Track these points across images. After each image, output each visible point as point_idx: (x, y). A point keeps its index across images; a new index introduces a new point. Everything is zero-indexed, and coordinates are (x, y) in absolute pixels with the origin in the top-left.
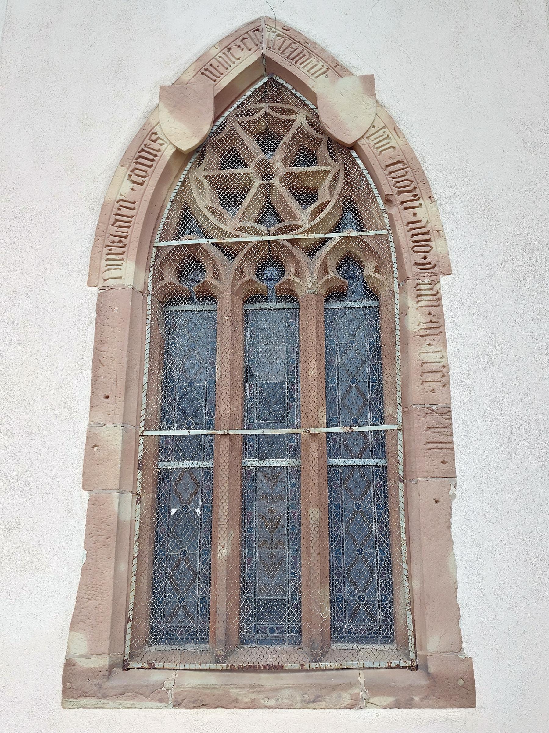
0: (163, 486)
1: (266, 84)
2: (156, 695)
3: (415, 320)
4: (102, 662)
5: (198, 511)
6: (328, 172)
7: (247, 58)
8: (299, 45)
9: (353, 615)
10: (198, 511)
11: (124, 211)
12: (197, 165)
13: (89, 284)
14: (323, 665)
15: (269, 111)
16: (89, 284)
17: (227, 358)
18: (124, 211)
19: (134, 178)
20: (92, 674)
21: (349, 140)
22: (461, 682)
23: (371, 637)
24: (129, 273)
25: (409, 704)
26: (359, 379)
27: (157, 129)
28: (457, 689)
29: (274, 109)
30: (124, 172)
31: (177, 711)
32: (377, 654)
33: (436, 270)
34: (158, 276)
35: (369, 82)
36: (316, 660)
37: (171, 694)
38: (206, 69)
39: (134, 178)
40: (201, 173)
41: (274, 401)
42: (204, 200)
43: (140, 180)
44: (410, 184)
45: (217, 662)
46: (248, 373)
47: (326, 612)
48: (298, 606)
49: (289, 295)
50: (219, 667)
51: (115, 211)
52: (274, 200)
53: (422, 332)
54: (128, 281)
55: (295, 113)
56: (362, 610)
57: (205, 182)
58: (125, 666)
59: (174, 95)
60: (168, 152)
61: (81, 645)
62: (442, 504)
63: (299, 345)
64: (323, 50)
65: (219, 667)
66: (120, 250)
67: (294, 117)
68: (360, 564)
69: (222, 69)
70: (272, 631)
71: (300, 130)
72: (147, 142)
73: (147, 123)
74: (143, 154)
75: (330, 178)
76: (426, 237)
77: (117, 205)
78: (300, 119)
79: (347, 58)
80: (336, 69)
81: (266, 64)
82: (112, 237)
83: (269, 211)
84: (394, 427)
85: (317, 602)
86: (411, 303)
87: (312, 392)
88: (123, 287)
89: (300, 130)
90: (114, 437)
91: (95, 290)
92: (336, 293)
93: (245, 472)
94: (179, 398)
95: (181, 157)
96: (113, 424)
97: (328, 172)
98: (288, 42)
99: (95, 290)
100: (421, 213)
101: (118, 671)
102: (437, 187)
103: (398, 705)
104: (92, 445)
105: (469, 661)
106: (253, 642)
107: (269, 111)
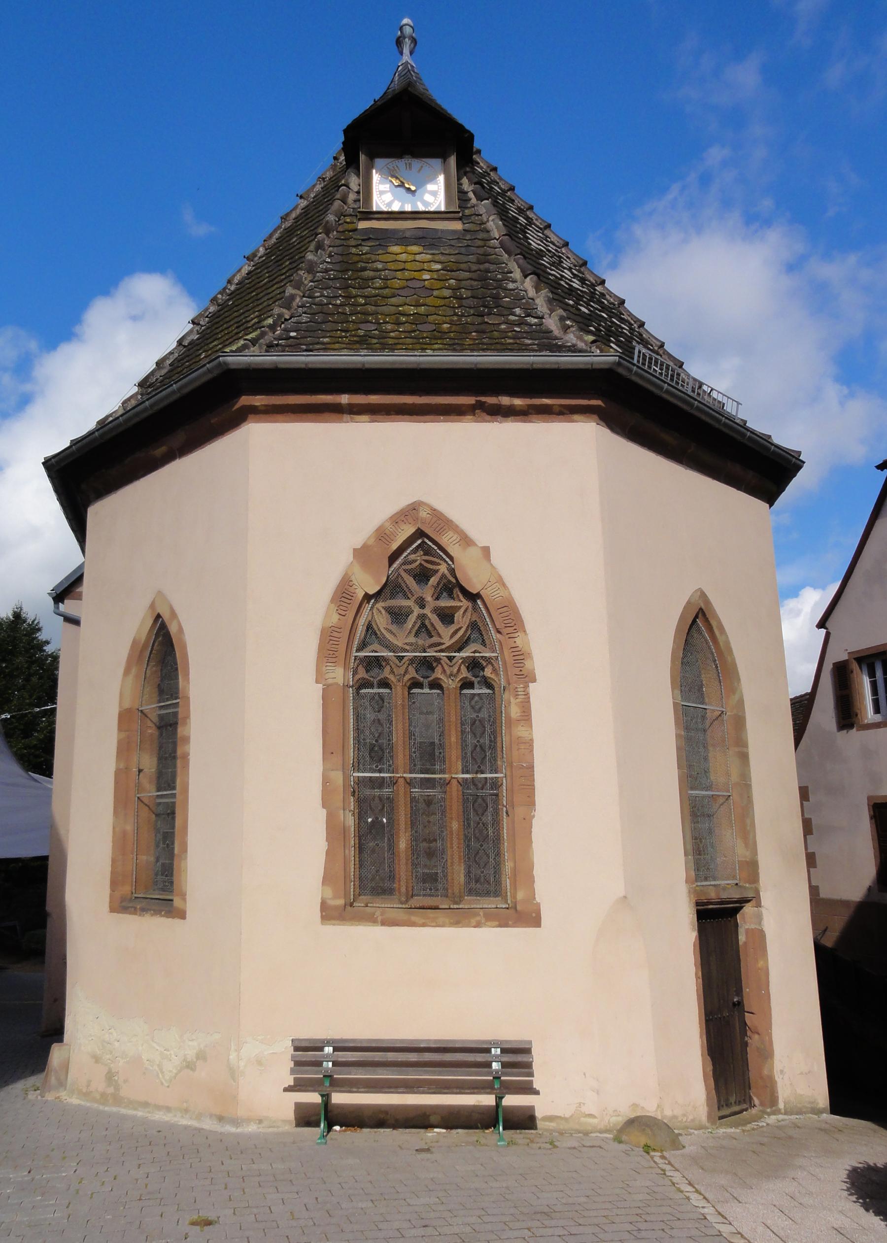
0: (363, 806)
1: (420, 544)
2: (371, 920)
3: (515, 711)
4: (341, 902)
5: (385, 820)
6: (460, 607)
7: (408, 530)
8: (442, 521)
9: (477, 881)
10: (385, 820)
11: (335, 634)
12: (376, 602)
13: (317, 682)
14: (461, 906)
15: (423, 562)
16: (317, 682)
17: (400, 726)
18: (335, 634)
19: (340, 611)
20: (336, 908)
21: (475, 592)
22: (534, 915)
23: (487, 894)
24: (339, 675)
25: (506, 925)
26: (482, 741)
27: (353, 578)
28: (531, 918)
29: (427, 561)
30: (334, 607)
31: (383, 927)
32: (490, 903)
33: (526, 679)
34: (355, 673)
35: (486, 551)
36: (456, 903)
37: (379, 919)
38: (382, 535)
39: (340, 611)
40: (380, 605)
41: (429, 755)
42: (382, 621)
43: (344, 613)
44: (513, 621)
45: (402, 903)
46: (411, 734)
47: (462, 879)
48: (445, 876)
49: (436, 685)
50: (404, 906)
51: (329, 634)
52: (427, 622)
53: (519, 718)
54: (340, 681)
55: (439, 564)
56: (482, 880)
57: (383, 612)
58: (351, 905)
59: (362, 554)
60: (360, 595)
61: (329, 893)
62: (528, 821)
63: (475, 871)
64: (457, 526)
65: (404, 906)
66: (334, 660)
67: (439, 567)
68: (481, 852)
69: (392, 537)
70: (431, 889)
71: (443, 575)
72: (346, 587)
73: (346, 574)
74: (344, 595)
75: (462, 610)
76: (521, 657)
77: (330, 630)
78: (443, 568)
79: (473, 533)
80: (466, 541)
81: (420, 533)
82: (328, 647)
83: (424, 629)
84: (502, 775)
85: (458, 874)
86: (512, 700)
87: (454, 753)
88: (337, 684)
89: (443, 575)
90: (338, 777)
91: (320, 686)
92: (467, 684)
93: (413, 800)
94: (373, 751)
95: (367, 597)
96: (337, 770)
97: (460, 607)
98: (435, 519)
99: (320, 686)
100: (519, 641)
101: (348, 908)
102: (528, 626)
103: (500, 926)
104: (326, 781)
105: (538, 905)
106: (420, 895)
107: (423, 562)
